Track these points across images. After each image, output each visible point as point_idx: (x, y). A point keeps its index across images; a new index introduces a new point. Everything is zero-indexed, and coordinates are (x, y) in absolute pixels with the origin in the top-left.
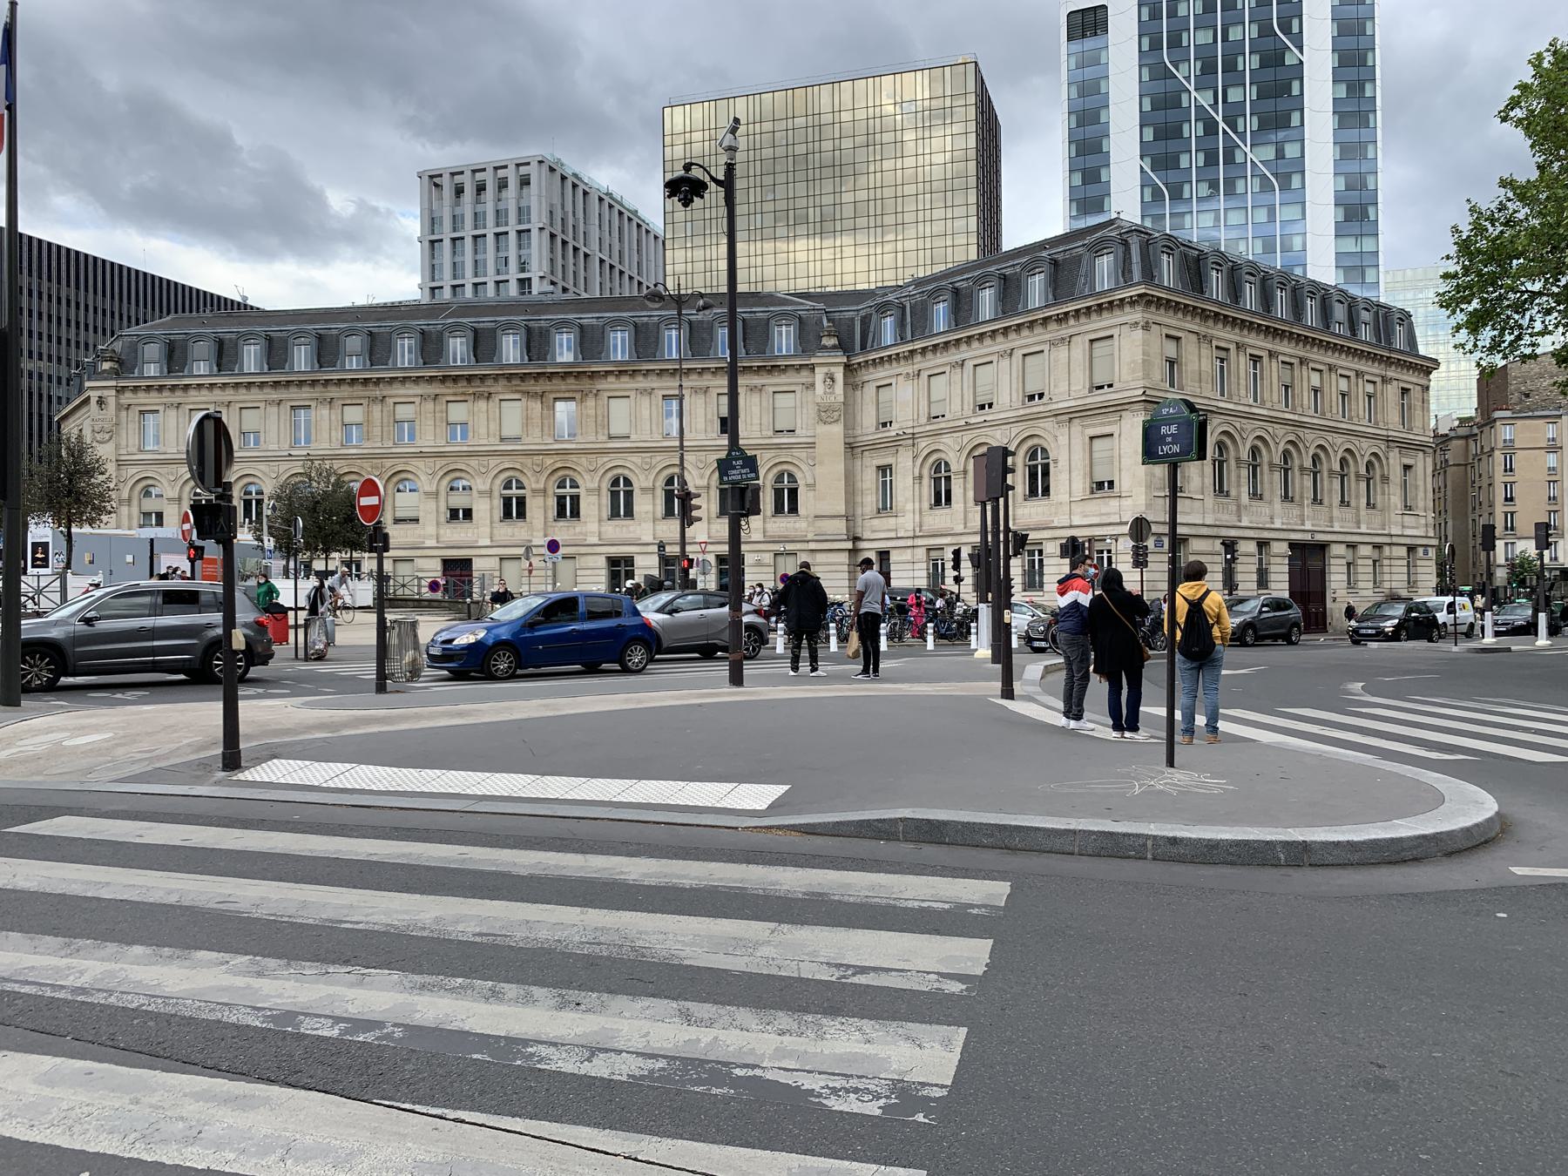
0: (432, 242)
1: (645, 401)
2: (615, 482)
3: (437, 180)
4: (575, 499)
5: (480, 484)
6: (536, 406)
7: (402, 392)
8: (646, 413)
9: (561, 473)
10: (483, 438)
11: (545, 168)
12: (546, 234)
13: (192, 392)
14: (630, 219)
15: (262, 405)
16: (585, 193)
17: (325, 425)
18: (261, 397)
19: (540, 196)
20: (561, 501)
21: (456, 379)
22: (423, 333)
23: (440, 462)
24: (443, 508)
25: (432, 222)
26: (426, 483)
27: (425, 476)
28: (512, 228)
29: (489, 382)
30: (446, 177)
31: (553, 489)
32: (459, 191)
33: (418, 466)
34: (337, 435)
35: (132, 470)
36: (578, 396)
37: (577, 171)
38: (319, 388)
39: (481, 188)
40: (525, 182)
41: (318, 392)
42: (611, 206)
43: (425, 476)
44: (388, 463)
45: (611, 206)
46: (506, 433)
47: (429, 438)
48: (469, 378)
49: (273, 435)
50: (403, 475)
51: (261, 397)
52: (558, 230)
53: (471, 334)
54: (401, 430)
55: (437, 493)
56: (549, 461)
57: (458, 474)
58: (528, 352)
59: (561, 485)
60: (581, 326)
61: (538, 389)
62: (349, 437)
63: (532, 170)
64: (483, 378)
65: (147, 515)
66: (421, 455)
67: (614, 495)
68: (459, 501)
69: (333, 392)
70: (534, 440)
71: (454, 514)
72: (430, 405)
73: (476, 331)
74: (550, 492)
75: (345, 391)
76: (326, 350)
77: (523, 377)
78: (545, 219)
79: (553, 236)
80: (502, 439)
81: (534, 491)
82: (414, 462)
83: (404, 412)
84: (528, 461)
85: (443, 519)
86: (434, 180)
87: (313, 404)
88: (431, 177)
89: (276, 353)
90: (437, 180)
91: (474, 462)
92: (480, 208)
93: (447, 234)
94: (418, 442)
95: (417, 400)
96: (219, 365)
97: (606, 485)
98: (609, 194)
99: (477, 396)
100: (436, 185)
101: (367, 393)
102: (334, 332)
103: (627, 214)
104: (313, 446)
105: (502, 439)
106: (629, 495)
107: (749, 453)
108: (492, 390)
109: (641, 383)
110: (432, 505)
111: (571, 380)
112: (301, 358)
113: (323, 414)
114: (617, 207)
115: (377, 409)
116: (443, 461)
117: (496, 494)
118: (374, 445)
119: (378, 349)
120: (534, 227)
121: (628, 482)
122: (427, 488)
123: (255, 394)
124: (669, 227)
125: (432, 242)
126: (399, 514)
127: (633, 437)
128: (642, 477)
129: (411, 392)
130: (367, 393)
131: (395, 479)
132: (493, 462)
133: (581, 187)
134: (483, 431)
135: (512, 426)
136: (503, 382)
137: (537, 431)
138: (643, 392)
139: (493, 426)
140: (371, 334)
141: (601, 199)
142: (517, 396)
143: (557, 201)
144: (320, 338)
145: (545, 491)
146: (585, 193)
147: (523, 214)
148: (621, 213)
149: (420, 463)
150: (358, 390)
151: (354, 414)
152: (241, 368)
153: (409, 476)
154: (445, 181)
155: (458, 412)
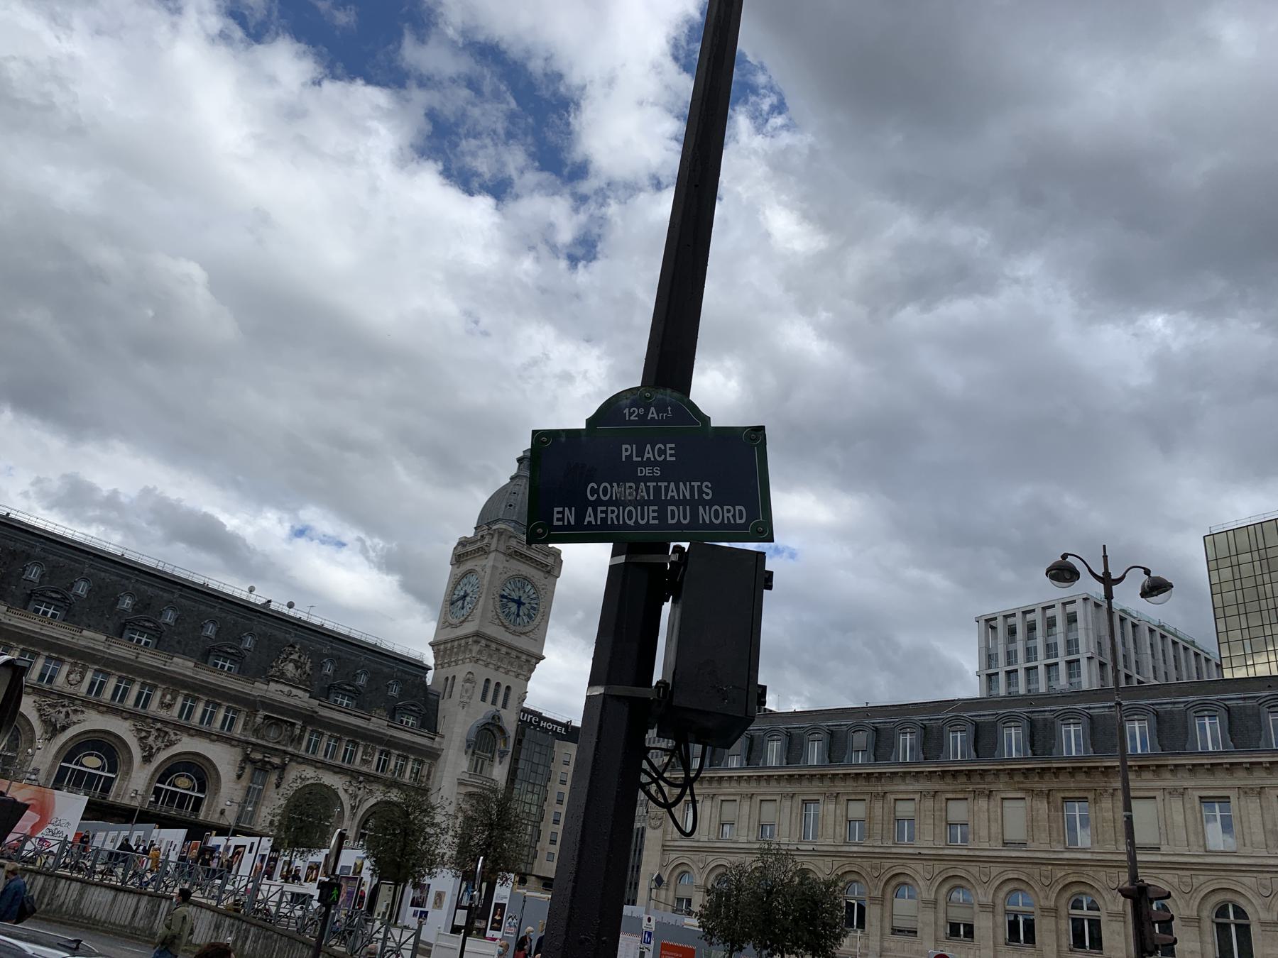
0: (989, 676)
1: (1176, 804)
2: (1222, 911)
3: (992, 623)
4: (1095, 924)
5: (983, 895)
6: (1042, 806)
7: (902, 787)
8: (1179, 818)
9: (1075, 889)
10: (985, 842)
11: (1090, 606)
12: (1095, 664)
13: (725, 784)
14: (1185, 649)
15: (778, 798)
16: (1134, 626)
17: (830, 820)
18: (777, 790)
19: (1087, 629)
20: (1077, 923)
21: (955, 774)
22: (925, 728)
23: (939, 866)
24: (942, 922)
25: (989, 657)
26: (926, 891)
27: (923, 880)
28: (1061, 660)
29: (990, 778)
30: (1000, 619)
31: (1066, 910)
32: (1012, 631)
33: (918, 870)
34: (841, 830)
35: (673, 856)
36: (1091, 796)
37: (1125, 606)
38: (827, 782)
39: (1031, 628)
40: (1072, 619)
41: (825, 787)
42: (1163, 637)
43: (923, 880)
44: (887, 863)
45: (1163, 637)
46: (1009, 836)
47: (928, 839)
48: (969, 774)
49: (785, 828)
50: (902, 879)
51: (777, 790)
52: (1108, 659)
53: (971, 729)
54: (901, 833)
55: (935, 902)
56: (1060, 873)
57: (958, 882)
58: (1032, 746)
59: (1077, 905)
60: (1091, 717)
61: (1044, 787)
62: (852, 834)
63: (1078, 608)
64: (983, 773)
65: (680, 900)
66: (919, 857)
67: (1223, 929)
68: (959, 915)
69: (840, 787)
70: (1041, 847)
71: (954, 928)
72: (929, 803)
73: (977, 725)
74: (1063, 912)
75: (850, 786)
76: (836, 745)
77: (1027, 773)
78: (1093, 649)
79: (1102, 665)
80: (1005, 844)
81: (1109, 914)
82: (912, 864)
83: (905, 809)
84: (1035, 871)
85: (942, 935)
86: (990, 623)
87: (821, 798)
88: (987, 621)
89: (794, 749)
90: (992, 623)
91: (974, 869)
92: (1031, 644)
93: (1002, 668)
94: (917, 843)
95: (917, 797)
96: (748, 759)
97: (1208, 913)
98: (1162, 627)
99: (977, 794)
100: (993, 628)
101: (870, 789)
102: (844, 728)
103: (1181, 643)
104: (819, 841)
105: (1005, 844)
106: (1244, 931)
107: (906, 639)
108: (993, 787)
109: (1169, 781)
110: (929, 916)
111: (1081, 777)
112: (814, 753)
113: (829, 809)
114: (1170, 637)
115: (878, 805)
116: (943, 865)
117: (1000, 909)
118: (875, 844)
119: (882, 743)
120: (1083, 656)
121: (1240, 912)
122: (925, 896)
123: (774, 788)
124: (1224, 647)
125: (989, 676)
126: (897, 924)
127: (1164, 849)
128: (1181, 903)
129: (911, 788)
130: (870, 789)
131: (894, 883)
132: (996, 870)
133: (1130, 620)
134: (984, 833)
135: (1016, 830)
136: (1004, 778)
137: (1044, 836)
138: (1173, 792)
139: (995, 828)
140: (877, 730)
141: (1151, 631)
142: (1019, 795)
143: (1105, 632)
144: (832, 734)
145: (1056, 910)
146: (1134, 626)
147: (1072, 645)
148: (1174, 643)
149: (919, 866)
150: (862, 786)
151: (857, 810)
152: (765, 762)
153: (908, 880)
154: (1000, 623)
155: (958, 811)
